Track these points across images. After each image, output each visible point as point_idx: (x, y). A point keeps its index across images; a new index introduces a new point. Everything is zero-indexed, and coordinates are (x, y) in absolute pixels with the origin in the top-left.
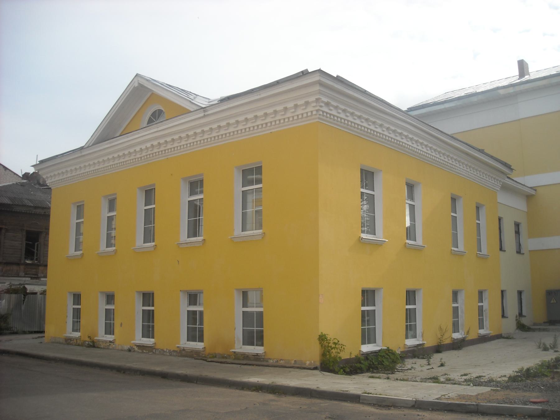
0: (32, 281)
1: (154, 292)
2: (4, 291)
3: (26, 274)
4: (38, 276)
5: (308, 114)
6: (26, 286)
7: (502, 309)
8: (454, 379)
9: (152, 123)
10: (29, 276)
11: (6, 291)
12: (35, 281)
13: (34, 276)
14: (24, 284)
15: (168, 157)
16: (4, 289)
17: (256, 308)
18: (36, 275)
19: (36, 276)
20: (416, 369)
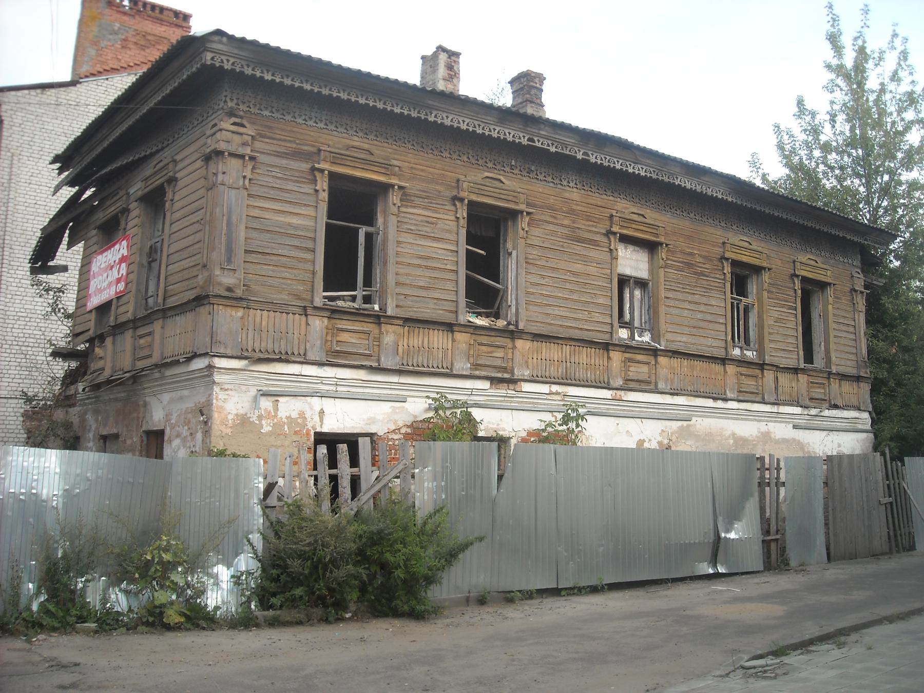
0: (493, 392)
2: (403, 431)
3: (476, 366)
4: (512, 373)
5: (318, 306)
6: (477, 413)
7: (701, 582)
8: (840, 48)
9: (497, 297)
10: (483, 373)
11: (409, 431)
12: (502, 391)
13: (499, 375)
14: (465, 405)
15: (643, 321)
16: (401, 424)
17: (763, 541)
18: (504, 369)
19: (506, 376)
20: (863, 7)
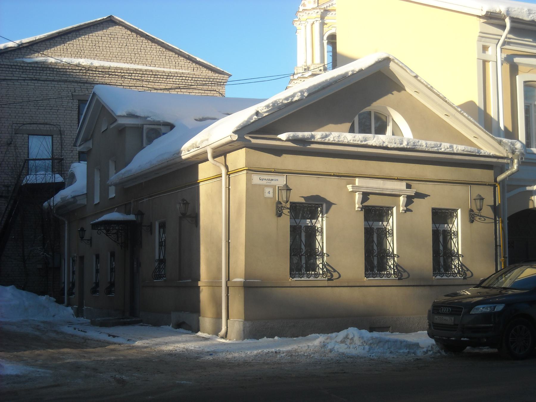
1: (476, 38)
17: (366, 229)
